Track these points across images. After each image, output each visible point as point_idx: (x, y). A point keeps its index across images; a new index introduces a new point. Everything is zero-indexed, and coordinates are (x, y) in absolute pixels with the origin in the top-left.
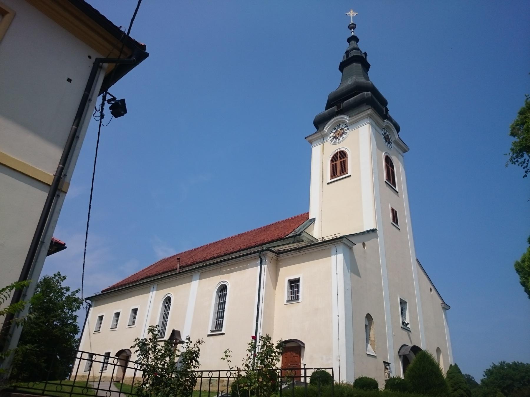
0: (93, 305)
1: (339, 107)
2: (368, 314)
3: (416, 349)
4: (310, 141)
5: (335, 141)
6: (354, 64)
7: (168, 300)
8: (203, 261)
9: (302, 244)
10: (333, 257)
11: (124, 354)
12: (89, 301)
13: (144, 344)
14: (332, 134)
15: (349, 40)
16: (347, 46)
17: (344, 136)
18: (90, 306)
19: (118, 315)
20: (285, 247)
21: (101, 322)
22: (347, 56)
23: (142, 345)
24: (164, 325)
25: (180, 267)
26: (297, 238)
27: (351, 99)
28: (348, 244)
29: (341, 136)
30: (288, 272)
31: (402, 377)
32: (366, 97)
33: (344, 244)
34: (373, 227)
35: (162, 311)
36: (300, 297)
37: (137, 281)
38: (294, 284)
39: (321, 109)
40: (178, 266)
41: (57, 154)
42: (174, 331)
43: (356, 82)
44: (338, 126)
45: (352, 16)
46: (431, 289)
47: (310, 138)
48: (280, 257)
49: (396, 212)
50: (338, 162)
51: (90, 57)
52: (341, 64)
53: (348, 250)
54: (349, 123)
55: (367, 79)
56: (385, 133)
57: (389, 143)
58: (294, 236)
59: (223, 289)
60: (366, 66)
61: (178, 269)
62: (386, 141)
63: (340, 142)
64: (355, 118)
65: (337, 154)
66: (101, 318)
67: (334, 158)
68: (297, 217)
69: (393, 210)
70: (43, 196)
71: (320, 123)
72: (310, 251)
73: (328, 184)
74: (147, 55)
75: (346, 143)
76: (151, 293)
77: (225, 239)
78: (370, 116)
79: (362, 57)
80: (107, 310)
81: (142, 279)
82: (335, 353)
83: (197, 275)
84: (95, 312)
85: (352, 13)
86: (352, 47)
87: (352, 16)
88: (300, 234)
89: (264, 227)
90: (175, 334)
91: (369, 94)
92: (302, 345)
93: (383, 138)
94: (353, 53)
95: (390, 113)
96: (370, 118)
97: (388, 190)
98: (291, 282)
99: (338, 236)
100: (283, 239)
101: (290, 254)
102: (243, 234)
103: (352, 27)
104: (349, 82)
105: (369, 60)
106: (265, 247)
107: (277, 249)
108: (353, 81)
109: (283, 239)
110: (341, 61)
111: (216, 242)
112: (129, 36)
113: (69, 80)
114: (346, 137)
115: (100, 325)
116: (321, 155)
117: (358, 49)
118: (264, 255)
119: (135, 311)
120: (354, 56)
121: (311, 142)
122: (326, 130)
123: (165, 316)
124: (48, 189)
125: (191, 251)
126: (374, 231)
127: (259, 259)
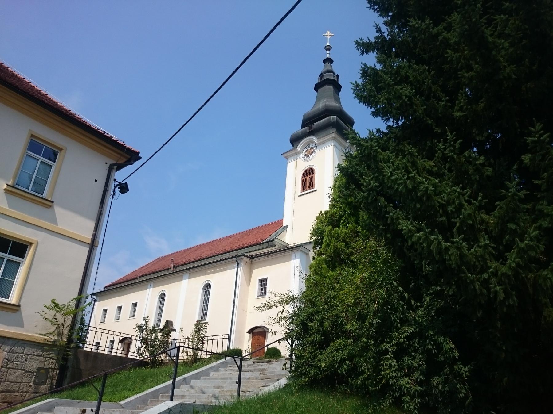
0: (97, 300)
1: (310, 128)
4: (287, 156)
5: (306, 159)
6: (327, 86)
7: (163, 296)
8: (194, 262)
9: (274, 249)
10: (293, 261)
11: (127, 341)
12: (94, 297)
13: (141, 327)
14: (304, 152)
15: (325, 62)
16: (321, 68)
17: (313, 154)
18: (95, 301)
19: (120, 308)
20: (258, 252)
21: (105, 315)
22: (321, 78)
23: (140, 328)
24: (160, 316)
25: (174, 266)
26: (270, 243)
29: (311, 154)
30: (259, 273)
32: (332, 121)
33: (301, 250)
35: (158, 305)
37: (136, 278)
38: (263, 282)
39: (297, 128)
40: (172, 265)
41: (92, 225)
42: (167, 321)
43: (325, 106)
44: (309, 145)
45: (328, 37)
47: (286, 155)
48: (254, 260)
50: (308, 178)
51: (106, 163)
52: (316, 85)
53: (305, 256)
55: (338, 100)
58: (268, 242)
60: (338, 88)
61: (172, 269)
63: (310, 160)
64: (322, 140)
65: (307, 170)
66: (105, 311)
67: (305, 174)
68: (275, 223)
70: (86, 250)
71: (295, 140)
73: (299, 196)
75: (314, 162)
76: (148, 290)
77: (215, 240)
78: (334, 139)
79: (334, 80)
80: (111, 304)
81: (140, 277)
83: (186, 275)
84: (99, 306)
85: (328, 35)
86: (326, 69)
87: (328, 37)
88: (273, 241)
89: (248, 231)
90: (169, 324)
91: (334, 118)
92: (266, 330)
94: (328, 76)
100: (260, 244)
101: (261, 259)
102: (230, 237)
103: (328, 48)
104: (321, 105)
105: (341, 82)
106: (241, 252)
107: (251, 254)
108: (324, 104)
109: (260, 244)
110: (316, 82)
111: (207, 243)
113: (96, 181)
114: (315, 156)
115: (105, 317)
116: (295, 169)
117: (331, 71)
118: (240, 259)
119: (135, 305)
120: (327, 79)
121: (287, 158)
122: (299, 148)
123: (161, 309)
124: (88, 246)
125: (185, 251)
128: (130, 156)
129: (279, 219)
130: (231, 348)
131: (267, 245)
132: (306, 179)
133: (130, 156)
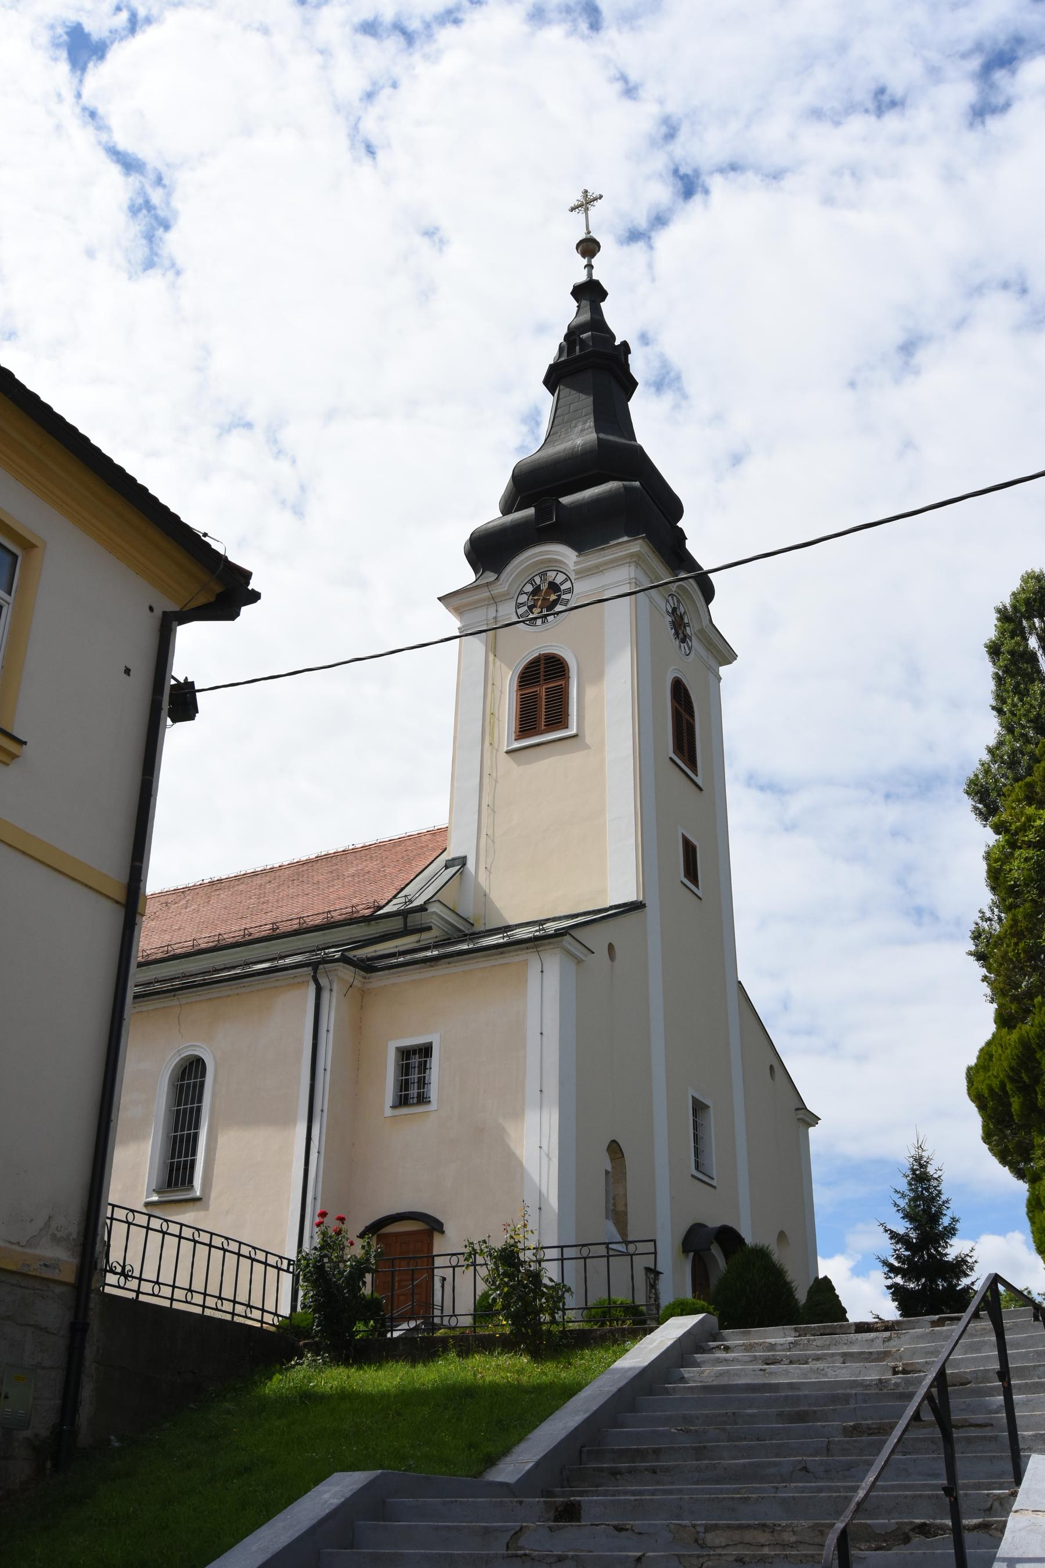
2: (614, 1141)
3: (728, 1237)
28: (577, 953)
34: (632, 898)
46: (771, 1067)
49: (694, 848)
50: (542, 690)
51: (151, 609)
54: (577, 572)
56: (674, 610)
57: (683, 641)
62: (677, 634)
64: (594, 558)
72: (467, 968)
74: (254, 597)
78: (636, 560)
88: (422, 908)
93: (669, 626)
96: (637, 564)
98: (405, 1053)
113: (127, 671)
126: (635, 907)
127: (312, 989)
128: (225, 590)
133: (225, 590)
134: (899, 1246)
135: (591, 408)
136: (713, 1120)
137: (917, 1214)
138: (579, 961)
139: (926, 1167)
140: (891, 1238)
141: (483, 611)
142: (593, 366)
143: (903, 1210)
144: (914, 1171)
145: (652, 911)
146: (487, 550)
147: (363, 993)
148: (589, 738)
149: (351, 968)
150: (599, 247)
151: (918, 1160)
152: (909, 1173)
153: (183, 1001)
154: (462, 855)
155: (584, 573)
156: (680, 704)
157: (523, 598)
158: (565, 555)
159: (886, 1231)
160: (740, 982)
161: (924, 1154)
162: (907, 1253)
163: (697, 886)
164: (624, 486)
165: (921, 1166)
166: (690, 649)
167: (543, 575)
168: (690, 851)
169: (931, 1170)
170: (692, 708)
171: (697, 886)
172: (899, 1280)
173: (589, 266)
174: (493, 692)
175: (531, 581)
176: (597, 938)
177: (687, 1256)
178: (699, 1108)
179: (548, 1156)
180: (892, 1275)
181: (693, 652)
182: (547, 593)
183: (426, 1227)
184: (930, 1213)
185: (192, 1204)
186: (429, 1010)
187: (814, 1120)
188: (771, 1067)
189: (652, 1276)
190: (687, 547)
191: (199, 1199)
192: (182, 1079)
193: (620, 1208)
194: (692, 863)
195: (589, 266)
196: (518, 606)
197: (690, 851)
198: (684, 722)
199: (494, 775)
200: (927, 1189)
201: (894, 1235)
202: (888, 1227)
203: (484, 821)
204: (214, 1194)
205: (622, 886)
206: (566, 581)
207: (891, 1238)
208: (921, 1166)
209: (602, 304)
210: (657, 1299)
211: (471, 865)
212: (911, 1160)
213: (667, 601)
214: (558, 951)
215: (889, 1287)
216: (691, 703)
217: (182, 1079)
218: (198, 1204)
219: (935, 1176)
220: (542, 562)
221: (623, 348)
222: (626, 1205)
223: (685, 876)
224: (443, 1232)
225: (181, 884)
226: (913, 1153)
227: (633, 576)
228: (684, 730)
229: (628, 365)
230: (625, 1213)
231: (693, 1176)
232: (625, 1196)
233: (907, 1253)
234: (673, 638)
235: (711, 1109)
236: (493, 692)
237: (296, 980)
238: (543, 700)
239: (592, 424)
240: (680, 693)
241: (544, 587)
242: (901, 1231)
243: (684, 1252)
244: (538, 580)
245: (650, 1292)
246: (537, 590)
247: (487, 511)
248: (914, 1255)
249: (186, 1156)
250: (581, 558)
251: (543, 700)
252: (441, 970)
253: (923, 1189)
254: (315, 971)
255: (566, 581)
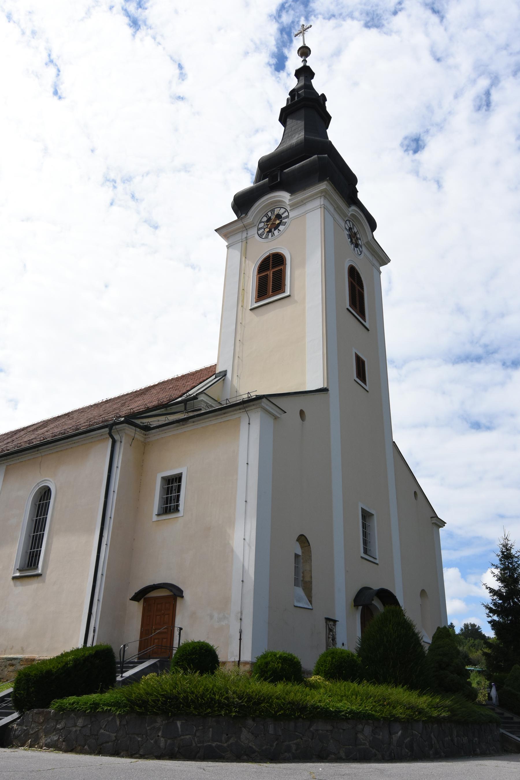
3: (386, 596)
17: (281, 228)
27: (297, 165)
31: (457, 631)
36: (181, 508)
46: (415, 493)
49: (363, 362)
50: (270, 273)
53: (270, 421)
54: (291, 206)
56: (350, 229)
58: (185, 402)
59: (44, 495)
62: (351, 241)
65: (268, 258)
67: (263, 267)
69: (356, 354)
78: (324, 194)
82: (235, 608)
88: (195, 398)
95: (360, 196)
97: (351, 322)
99: (253, 395)
111: (58, 417)
112: (237, 218)
114: (285, 230)
118: (118, 432)
127: (110, 440)
129: (230, 249)
130: (89, 644)
131: (181, 407)
132: (267, 275)
134: (495, 597)
135: (303, 127)
136: (376, 524)
137: (505, 578)
138: (276, 418)
139: (510, 550)
140: (490, 592)
141: (240, 234)
142: (306, 108)
143: (497, 576)
144: (503, 552)
145: (334, 394)
146: (242, 203)
147: (145, 444)
148: (296, 296)
149: (134, 428)
150: (310, 51)
151: (505, 546)
152: (500, 553)
153: (43, 454)
154: (224, 369)
155: (295, 206)
156: (355, 281)
157: (262, 225)
158: (284, 196)
159: (487, 588)
160: (394, 442)
161: (509, 542)
162: (500, 602)
163: (365, 384)
164: (318, 157)
165: (507, 550)
166: (361, 252)
167: (273, 211)
168: (360, 364)
169: (513, 552)
170: (362, 284)
171: (365, 384)
172: (496, 618)
173: (305, 61)
174: (244, 278)
175: (266, 215)
176: (292, 407)
177: (357, 608)
178: (366, 515)
179: (249, 545)
180: (491, 615)
181: (363, 254)
182: (275, 220)
183: (171, 593)
184: (514, 577)
185: (36, 578)
186: (188, 456)
187: (442, 523)
188: (415, 493)
189: (331, 623)
190: (328, 109)
191: (39, 575)
192: (40, 501)
193: (307, 579)
194: (362, 368)
195: (305, 61)
196: (259, 229)
197: (360, 364)
198: (357, 292)
199: (243, 323)
200: (511, 563)
201: (492, 591)
202: (488, 586)
203: (237, 349)
204: (48, 572)
205: (315, 380)
206: (285, 212)
207: (490, 592)
208: (507, 550)
209: (312, 81)
210: (334, 639)
211: (229, 375)
212: (501, 546)
213: (346, 223)
214: (259, 409)
215: (490, 622)
216: (362, 281)
217: (40, 501)
218: (40, 578)
219: (516, 555)
220: (272, 203)
221: (321, 97)
222: (311, 577)
223: (357, 377)
224: (183, 597)
225: (92, 403)
226: (502, 542)
227: (322, 203)
228: (357, 296)
229: (325, 107)
230: (311, 582)
231: (362, 557)
232: (311, 571)
233: (500, 602)
234: (350, 244)
235: (375, 516)
236: (244, 278)
237: (102, 437)
238: (271, 278)
239: (303, 134)
240: (354, 274)
241: (273, 217)
242: (496, 588)
243: (355, 606)
244: (270, 214)
245: (329, 634)
246: (269, 219)
247: (247, 182)
248: (504, 602)
249: (38, 548)
250: (293, 197)
251: (271, 278)
252: (189, 428)
253: (509, 563)
254: (110, 430)
255: (285, 212)
